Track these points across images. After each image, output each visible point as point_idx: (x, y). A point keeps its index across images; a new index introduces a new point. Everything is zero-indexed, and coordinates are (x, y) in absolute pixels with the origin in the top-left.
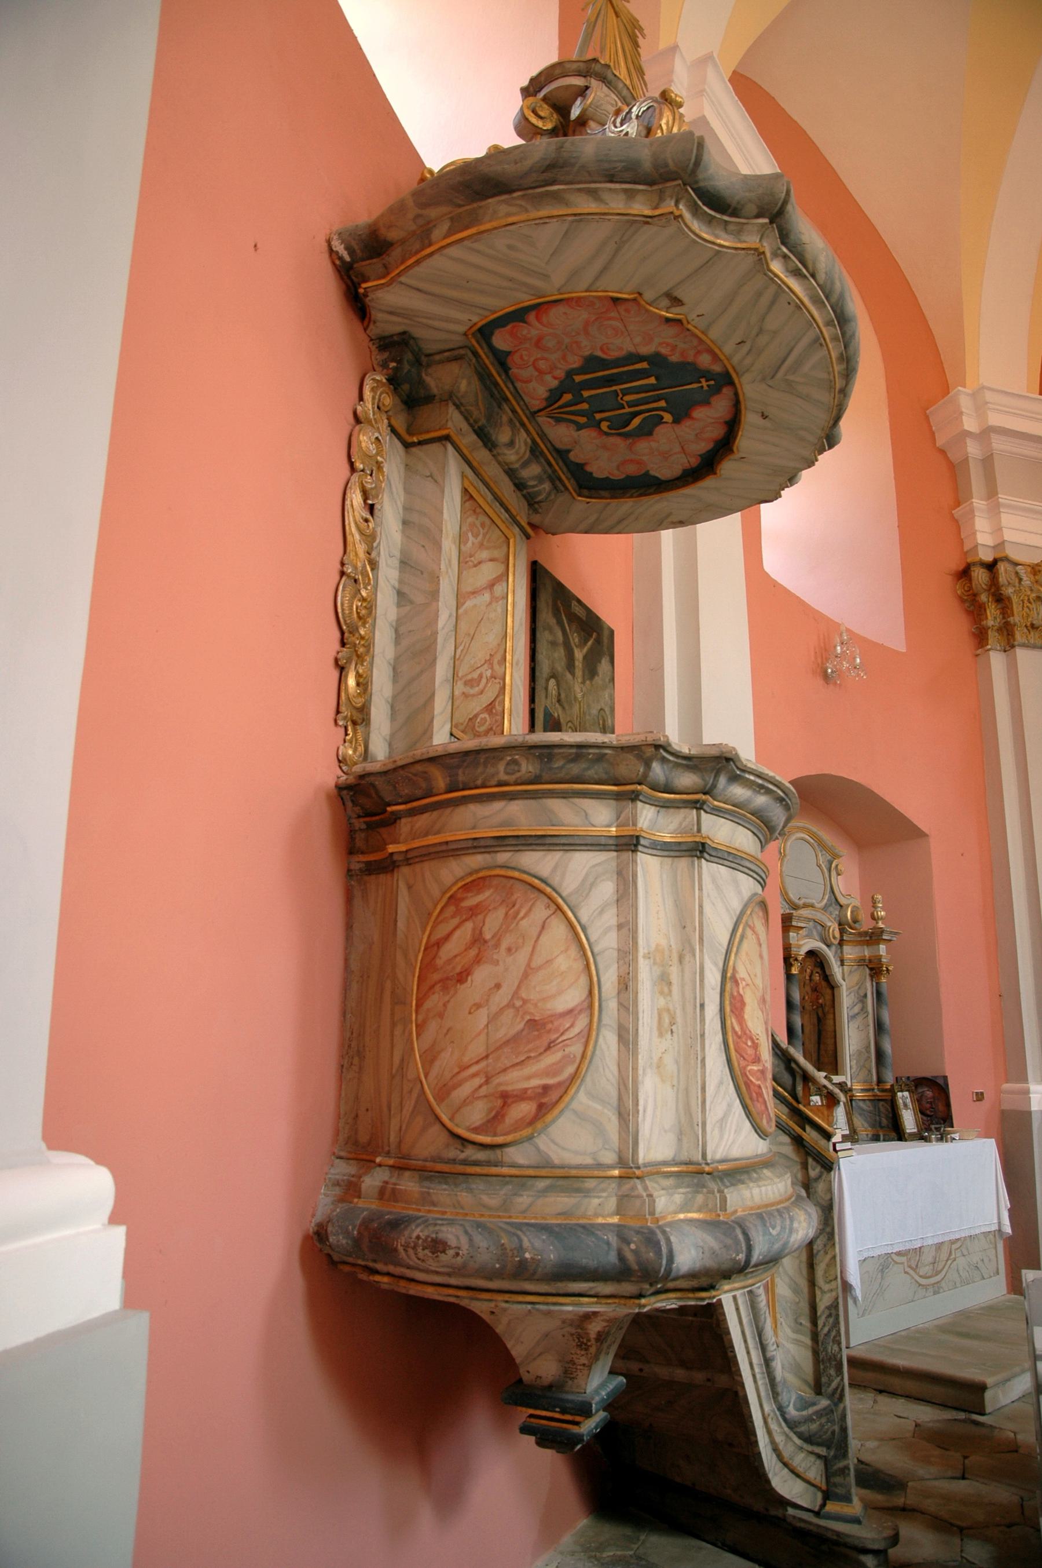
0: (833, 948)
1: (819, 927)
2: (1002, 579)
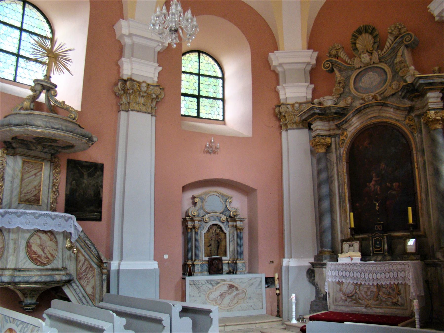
0: (225, 223)
1: (219, 218)
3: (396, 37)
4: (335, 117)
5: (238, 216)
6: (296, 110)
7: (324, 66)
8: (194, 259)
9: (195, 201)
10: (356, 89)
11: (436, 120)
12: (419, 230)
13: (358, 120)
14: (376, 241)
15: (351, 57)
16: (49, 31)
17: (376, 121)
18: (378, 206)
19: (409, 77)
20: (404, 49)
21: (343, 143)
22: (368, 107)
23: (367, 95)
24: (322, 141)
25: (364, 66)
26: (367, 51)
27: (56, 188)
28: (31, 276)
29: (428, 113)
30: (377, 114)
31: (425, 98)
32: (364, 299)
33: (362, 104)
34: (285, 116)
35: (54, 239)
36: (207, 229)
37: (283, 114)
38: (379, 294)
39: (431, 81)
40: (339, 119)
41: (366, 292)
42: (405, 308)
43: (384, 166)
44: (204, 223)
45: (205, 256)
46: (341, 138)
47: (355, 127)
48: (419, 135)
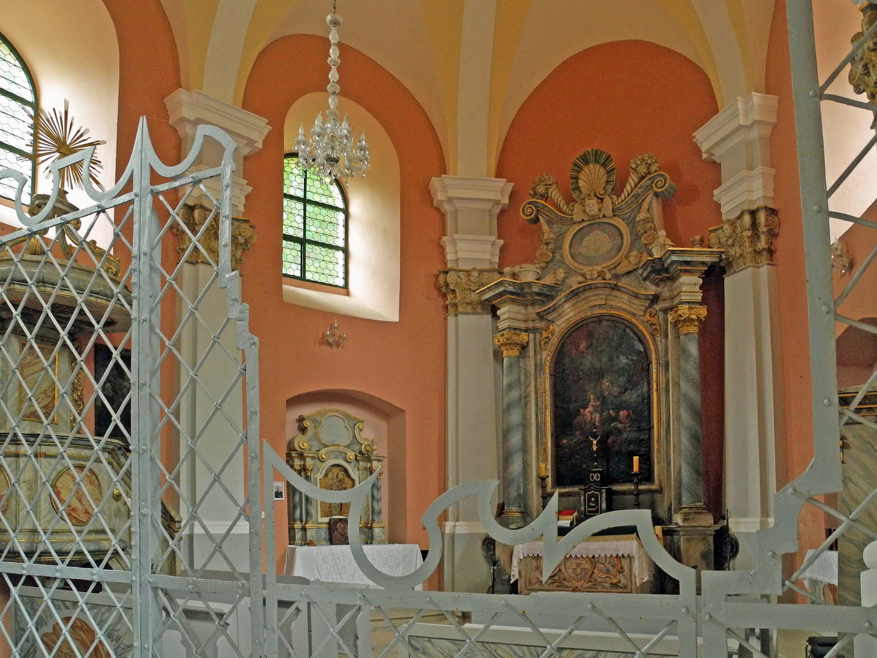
0: (353, 464)
1: (343, 455)
3: (643, 178)
4: (537, 300)
5: (375, 452)
8: (304, 520)
9: (305, 425)
11: (689, 320)
15: (570, 200)
16: (28, 85)
17: (601, 312)
18: (597, 444)
19: (657, 247)
20: (652, 199)
21: (546, 343)
23: (590, 268)
24: (515, 338)
26: (596, 196)
27: (79, 394)
28: (63, 542)
30: (603, 302)
31: (677, 284)
34: (453, 291)
35: (96, 482)
36: (324, 472)
37: (452, 287)
38: (593, 572)
39: (689, 259)
40: (543, 303)
41: (574, 570)
42: (629, 591)
44: (319, 463)
45: (322, 517)
47: (567, 320)
48: (663, 340)
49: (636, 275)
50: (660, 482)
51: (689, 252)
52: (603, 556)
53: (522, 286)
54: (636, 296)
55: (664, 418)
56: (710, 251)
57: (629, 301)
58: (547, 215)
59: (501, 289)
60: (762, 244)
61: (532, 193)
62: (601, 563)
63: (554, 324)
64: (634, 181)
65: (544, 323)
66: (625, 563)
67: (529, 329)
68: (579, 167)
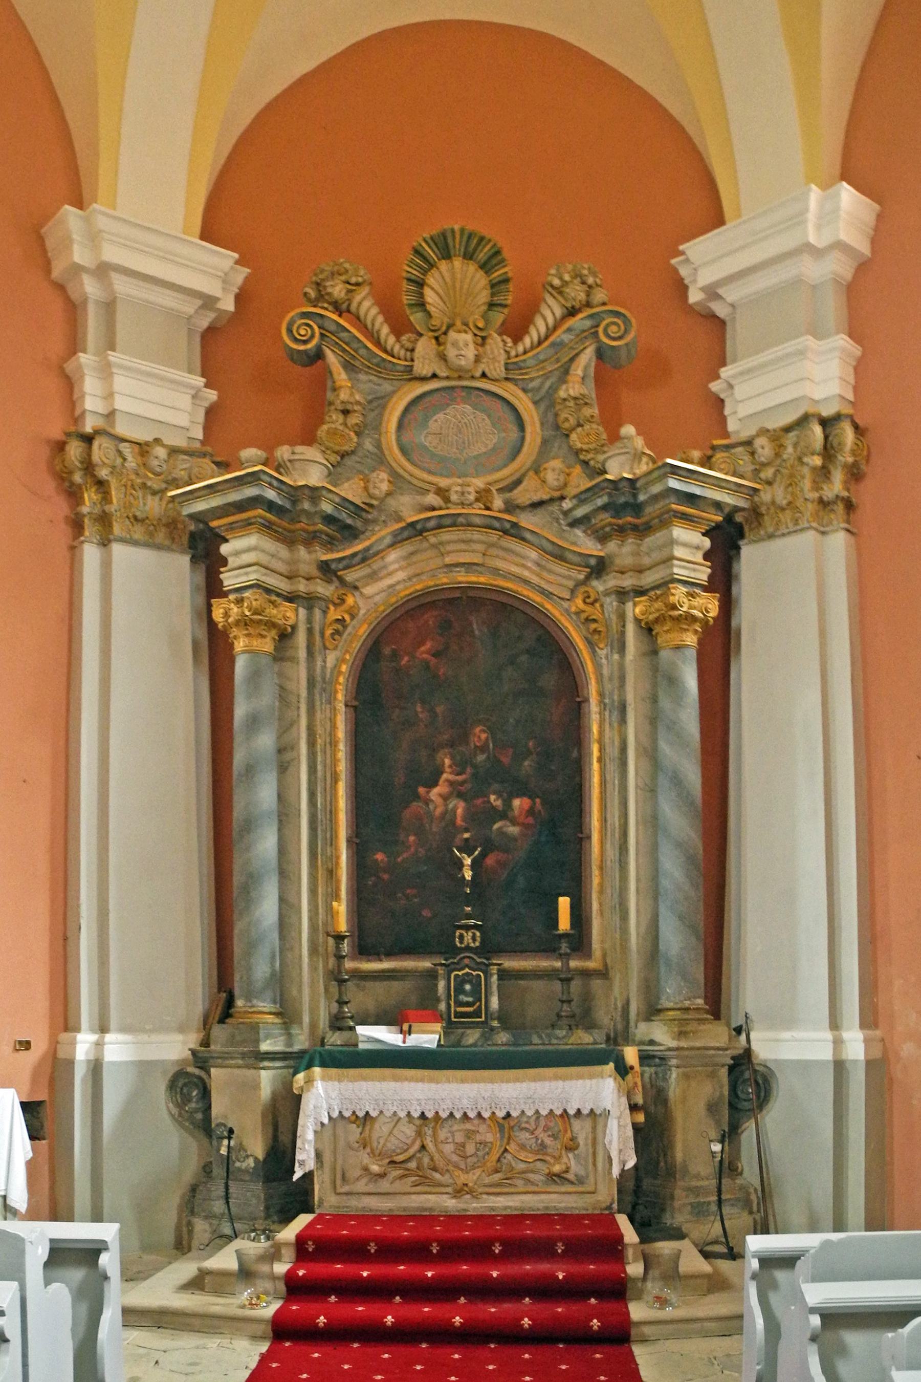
2: (97, 455)
3: (572, 312)
6: (158, 469)
7: (289, 331)
10: (404, 451)
12: (588, 955)
13: (403, 563)
14: (461, 982)
15: (400, 327)
19: (623, 458)
21: (337, 632)
22: (454, 525)
24: (272, 612)
25: (448, 378)
29: (673, 591)
32: (450, 1168)
33: (434, 509)
39: (697, 491)
40: (330, 543)
42: (591, 1189)
43: (484, 736)
46: (334, 614)
48: (616, 657)
49: (552, 513)
50: (604, 956)
51: (701, 478)
52: (530, 1113)
53: (295, 493)
54: (559, 555)
55: (614, 818)
56: (736, 484)
57: (538, 565)
58: (344, 350)
59: (250, 492)
60: (836, 486)
61: (313, 294)
62: (526, 1129)
63: (357, 594)
64: (554, 314)
65: (332, 588)
66: (581, 1130)
67: (299, 596)
68: (425, 259)
